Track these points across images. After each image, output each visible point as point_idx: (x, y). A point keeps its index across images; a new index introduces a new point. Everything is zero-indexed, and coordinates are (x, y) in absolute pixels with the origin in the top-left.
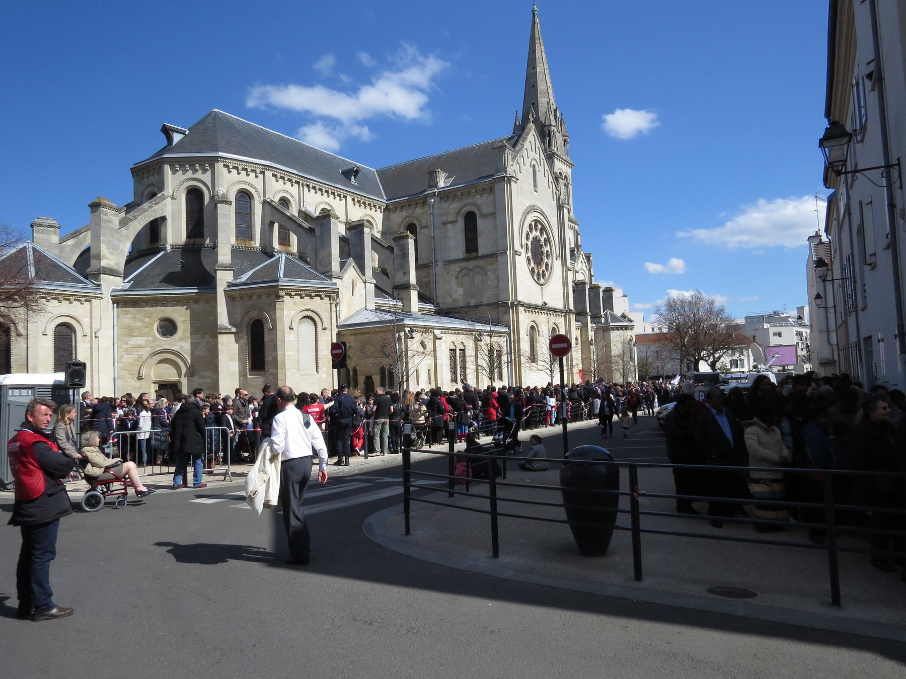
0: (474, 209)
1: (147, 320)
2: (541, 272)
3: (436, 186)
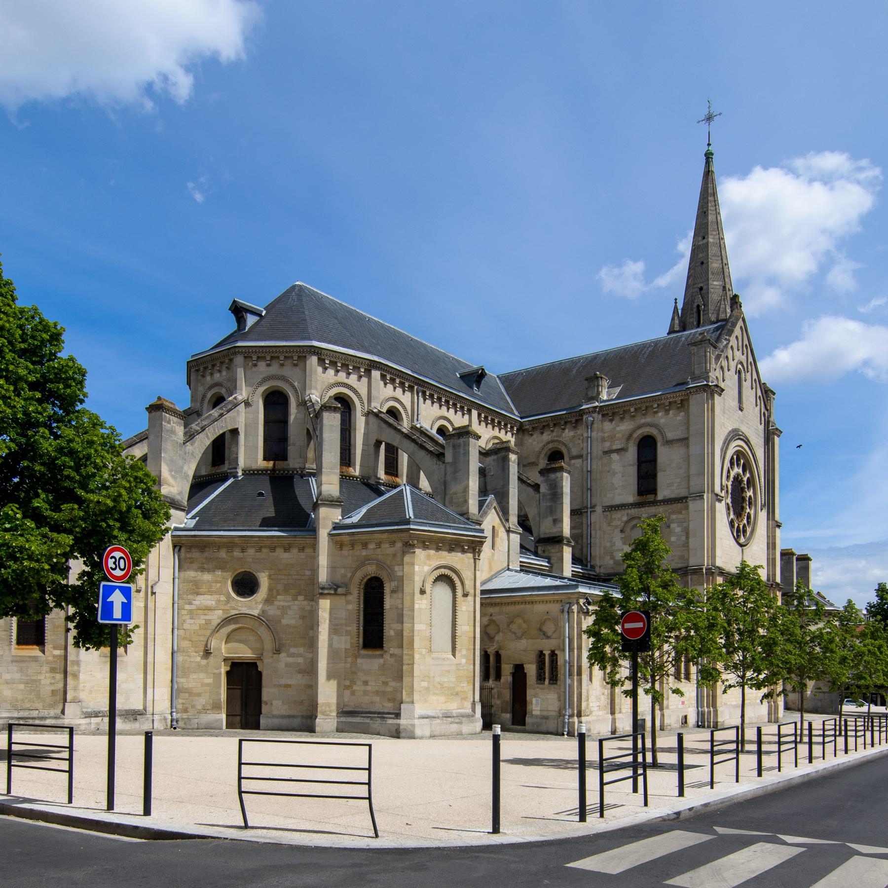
0: (654, 432)
2: (741, 526)
3: (596, 398)
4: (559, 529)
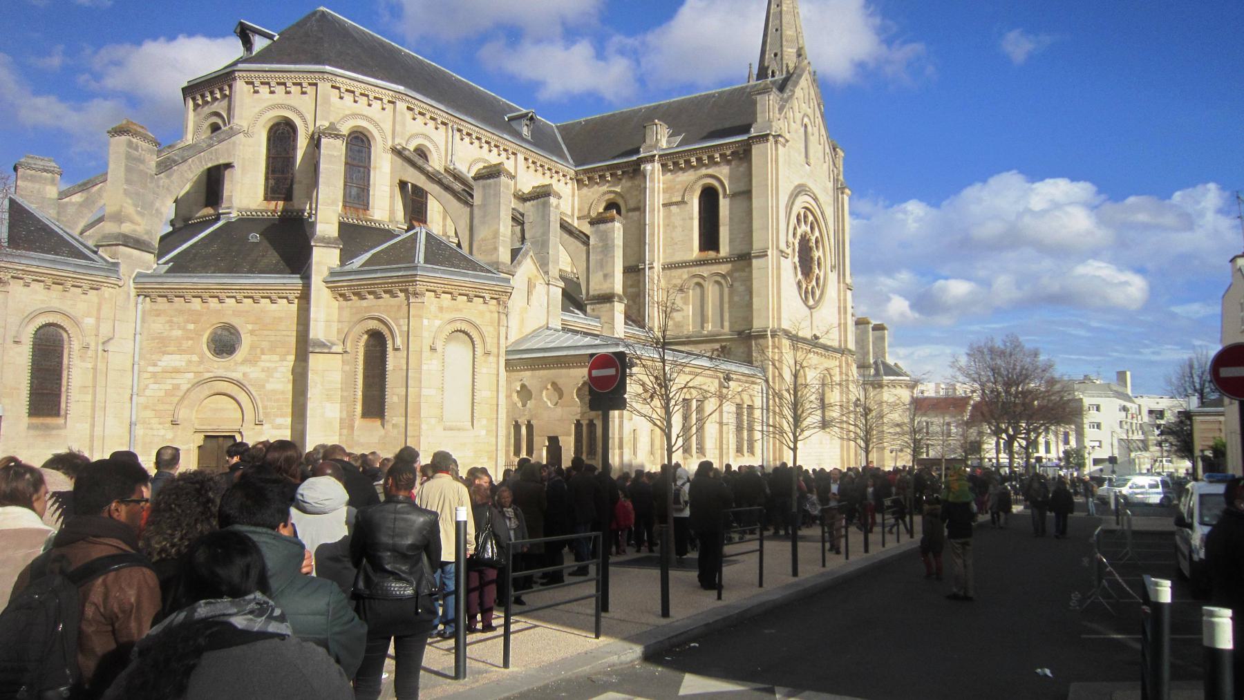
1: (191, 326)
2: (810, 288)
4: (611, 286)
